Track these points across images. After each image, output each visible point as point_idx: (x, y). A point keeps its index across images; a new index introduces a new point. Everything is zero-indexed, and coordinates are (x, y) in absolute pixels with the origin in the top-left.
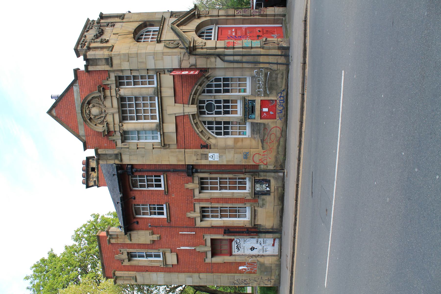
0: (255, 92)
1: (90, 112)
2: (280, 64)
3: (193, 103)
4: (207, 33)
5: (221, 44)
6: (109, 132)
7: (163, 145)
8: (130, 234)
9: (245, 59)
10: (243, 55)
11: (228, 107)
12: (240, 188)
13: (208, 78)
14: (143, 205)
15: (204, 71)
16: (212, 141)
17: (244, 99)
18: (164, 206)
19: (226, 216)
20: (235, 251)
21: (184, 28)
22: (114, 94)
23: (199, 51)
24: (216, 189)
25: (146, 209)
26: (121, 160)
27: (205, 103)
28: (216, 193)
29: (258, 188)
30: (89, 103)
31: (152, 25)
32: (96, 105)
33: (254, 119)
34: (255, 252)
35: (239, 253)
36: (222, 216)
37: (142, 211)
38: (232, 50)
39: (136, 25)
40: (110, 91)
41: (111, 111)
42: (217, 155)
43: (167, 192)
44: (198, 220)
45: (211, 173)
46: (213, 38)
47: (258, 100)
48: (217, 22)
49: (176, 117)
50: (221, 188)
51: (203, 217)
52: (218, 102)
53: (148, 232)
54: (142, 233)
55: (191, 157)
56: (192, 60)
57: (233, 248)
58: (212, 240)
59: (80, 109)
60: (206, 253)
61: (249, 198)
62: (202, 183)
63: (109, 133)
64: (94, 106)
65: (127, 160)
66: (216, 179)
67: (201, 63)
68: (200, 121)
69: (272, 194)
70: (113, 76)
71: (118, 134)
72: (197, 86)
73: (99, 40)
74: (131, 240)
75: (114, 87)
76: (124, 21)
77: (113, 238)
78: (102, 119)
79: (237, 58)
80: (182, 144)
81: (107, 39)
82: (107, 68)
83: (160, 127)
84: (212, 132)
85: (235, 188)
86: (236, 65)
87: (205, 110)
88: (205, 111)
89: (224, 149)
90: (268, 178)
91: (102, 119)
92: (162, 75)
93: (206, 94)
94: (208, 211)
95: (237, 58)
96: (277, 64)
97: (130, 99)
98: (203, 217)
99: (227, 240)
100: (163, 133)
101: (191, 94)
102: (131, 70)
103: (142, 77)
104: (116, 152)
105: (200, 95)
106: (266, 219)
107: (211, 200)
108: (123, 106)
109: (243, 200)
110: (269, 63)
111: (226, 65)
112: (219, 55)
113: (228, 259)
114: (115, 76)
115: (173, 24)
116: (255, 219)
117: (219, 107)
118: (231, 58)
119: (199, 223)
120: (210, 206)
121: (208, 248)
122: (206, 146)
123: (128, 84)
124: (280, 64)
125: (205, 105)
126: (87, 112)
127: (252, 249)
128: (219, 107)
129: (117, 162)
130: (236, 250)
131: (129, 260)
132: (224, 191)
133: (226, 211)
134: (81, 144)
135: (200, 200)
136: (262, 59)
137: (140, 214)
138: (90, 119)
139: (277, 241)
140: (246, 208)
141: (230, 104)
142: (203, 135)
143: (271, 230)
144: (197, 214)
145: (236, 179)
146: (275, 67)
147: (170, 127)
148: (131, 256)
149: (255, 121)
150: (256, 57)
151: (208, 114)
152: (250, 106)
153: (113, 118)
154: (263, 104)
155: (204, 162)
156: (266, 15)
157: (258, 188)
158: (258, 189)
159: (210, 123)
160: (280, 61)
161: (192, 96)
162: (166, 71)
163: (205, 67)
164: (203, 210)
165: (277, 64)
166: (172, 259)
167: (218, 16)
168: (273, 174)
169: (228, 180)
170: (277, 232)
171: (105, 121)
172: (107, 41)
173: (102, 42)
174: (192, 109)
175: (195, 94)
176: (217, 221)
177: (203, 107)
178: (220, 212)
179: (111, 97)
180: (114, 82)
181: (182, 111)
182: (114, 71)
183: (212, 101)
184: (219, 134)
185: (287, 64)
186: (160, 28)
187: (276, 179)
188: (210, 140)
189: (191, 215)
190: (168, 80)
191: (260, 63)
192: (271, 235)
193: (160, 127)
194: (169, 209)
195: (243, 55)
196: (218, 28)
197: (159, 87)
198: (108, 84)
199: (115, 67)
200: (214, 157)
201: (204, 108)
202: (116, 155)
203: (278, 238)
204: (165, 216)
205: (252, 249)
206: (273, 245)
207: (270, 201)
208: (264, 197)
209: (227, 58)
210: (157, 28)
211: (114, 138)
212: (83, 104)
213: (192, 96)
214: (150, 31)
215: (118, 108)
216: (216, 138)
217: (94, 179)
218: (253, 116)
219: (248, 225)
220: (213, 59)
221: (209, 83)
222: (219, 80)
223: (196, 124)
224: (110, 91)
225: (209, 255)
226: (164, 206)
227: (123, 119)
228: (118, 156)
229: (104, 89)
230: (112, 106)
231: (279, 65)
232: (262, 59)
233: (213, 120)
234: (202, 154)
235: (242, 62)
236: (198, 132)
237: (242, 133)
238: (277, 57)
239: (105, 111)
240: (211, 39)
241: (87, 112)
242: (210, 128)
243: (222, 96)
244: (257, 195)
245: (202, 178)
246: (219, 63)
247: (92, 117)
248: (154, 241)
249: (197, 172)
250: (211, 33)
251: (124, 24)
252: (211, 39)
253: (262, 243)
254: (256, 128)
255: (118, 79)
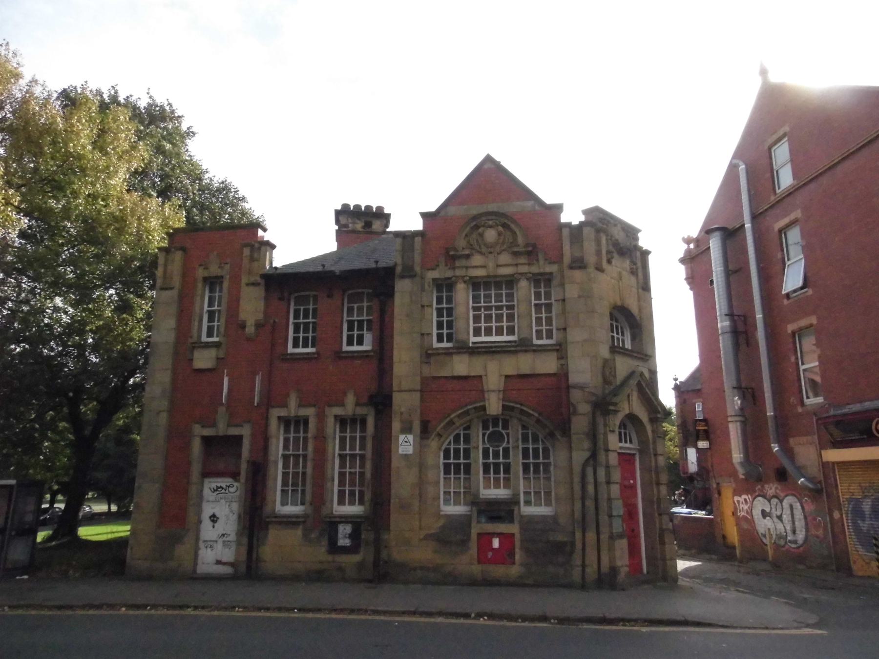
0: (529, 523)
1: (491, 227)
2: (583, 571)
3: (504, 407)
4: (625, 434)
5: (613, 459)
6: (454, 258)
7: (430, 352)
8: (259, 284)
9: (590, 504)
10: (596, 500)
11: (497, 472)
12: (341, 494)
13: (551, 435)
14: (315, 310)
15: (565, 428)
16: (433, 443)
17: (514, 501)
18: (310, 350)
19: (286, 466)
20: (210, 484)
21: (635, 396)
22: (524, 269)
23: (600, 421)
24: (342, 447)
25: (306, 316)
26: (402, 277)
27: (503, 428)
28: (334, 448)
29: (344, 530)
30: (505, 226)
31: (633, 338)
32: (502, 238)
33: (478, 522)
34: (206, 524)
35: (207, 492)
36: (286, 458)
37: (302, 308)
38: (604, 480)
39: (635, 310)
40: (525, 264)
41: (491, 265)
42: (410, 450)
43: (340, 356)
44: (283, 413)
45: (375, 438)
46: (623, 445)
47: (513, 529)
48: (643, 451)
49: (481, 377)
50: (342, 457)
51: (286, 422)
52: (506, 451)
53: (261, 316)
54: (261, 305)
55: (405, 402)
56: (584, 408)
57: (219, 480)
58: (239, 439)
59: (495, 210)
60: (214, 425)
61: (325, 511)
62: (353, 420)
63: (452, 258)
64: (500, 234)
65: (402, 288)
66: (363, 447)
67: (580, 424)
68: (470, 421)
69: (330, 558)
70: (553, 268)
71: (449, 274)
72: (536, 415)
73: (611, 248)
74: (248, 285)
75: (535, 269)
76: (640, 290)
77: (252, 251)
78: (478, 248)
79: (591, 488)
80: (429, 387)
81: (614, 261)
82: (567, 260)
83: (464, 349)
84: (450, 442)
85: (342, 483)
86: (577, 488)
87: (491, 429)
88: (488, 429)
89: (419, 462)
90: (362, 549)
91: (478, 248)
92: (555, 354)
93: (520, 432)
94: (297, 431)
95: (591, 488)
96: (584, 566)
97: (510, 297)
98: (286, 422)
99: (238, 467)
100: (451, 354)
101: (522, 405)
102: (564, 300)
103: (549, 321)
104: (417, 269)
105: (520, 420)
106: (282, 547)
107: (321, 437)
108: (498, 285)
109: (319, 500)
110: (584, 549)
111: (577, 469)
112: (594, 456)
113: (196, 469)
114: (551, 274)
115: (642, 374)
116: (280, 523)
117: (496, 455)
118: (590, 478)
119: (276, 413)
120: (310, 435)
121: (222, 428)
122: (425, 431)
123: (538, 296)
124: (583, 571)
125: (500, 429)
126: (490, 223)
127: (214, 519)
128: (496, 455)
129: (399, 269)
130: (214, 485)
131: (205, 279)
132: (337, 461)
133: (296, 465)
134: (433, 208)
135: (321, 417)
136: (591, 536)
137: (295, 305)
138: (477, 227)
139: (228, 570)
140: (303, 504)
141: (502, 475)
142: (448, 424)
143: (254, 556)
144: (293, 408)
145: (362, 484)
146: (577, 560)
147: (461, 366)
148: (213, 282)
149: (474, 524)
150: (594, 526)
151: (484, 435)
152: (503, 514)
153: (479, 266)
154: (506, 538)
155: (396, 425)
156: (662, 543)
157: (344, 530)
158: (341, 528)
159: (467, 439)
160: (588, 570)
161: (519, 406)
162: (563, 362)
163: (573, 431)
164: (301, 422)
165: (584, 566)
166: (203, 360)
167: (655, 455)
168: (370, 558)
169: (358, 470)
170: (249, 569)
171: (473, 251)
172: (609, 262)
173: (609, 252)
174: (494, 406)
175: (522, 412)
176: (277, 448)
177: (495, 425)
178: (293, 455)
179: (517, 265)
180: (542, 271)
181: (492, 387)
182: (561, 271)
183: (508, 442)
184: (447, 455)
185: (583, 586)
186: (627, 350)
187: (361, 566)
188: (437, 439)
189: (293, 402)
190: (548, 365)
191: (584, 532)
192: (244, 557)
193: (464, 349)
194: (307, 358)
195: (596, 500)
196: (634, 455)
197: (534, 348)
198: (538, 260)
199: (568, 273)
200: (405, 444)
201: (494, 428)
202: (411, 268)
203: (236, 571)
204: (291, 350)
205: (214, 519)
206: (219, 562)
207: (316, 555)
208: (325, 542)
209: (590, 471)
210: (628, 345)
211: (442, 266)
212: (504, 215)
213: (519, 406)
214: (623, 334)
215: (495, 276)
216: (440, 449)
217: (350, 225)
218: (483, 520)
219: (267, 509)
220: (587, 444)
221: (541, 437)
222: (546, 455)
223: (467, 413)
224: (525, 264)
225: (208, 432)
226: (310, 350)
227: (476, 284)
228: (409, 273)
229: (529, 253)
230: (504, 265)
231: (580, 569)
232: (591, 536)
233: (473, 444)
234: (411, 423)
235: (583, 498)
236: (452, 416)
237: (448, 497)
238: (595, 566)
239: (491, 253)
240: (620, 441)
241: (490, 223)
242: (457, 439)
243: (517, 461)
244: (332, 524)
245: (363, 422)
246: (580, 456)
247: (480, 230)
248: (243, 326)
249: (378, 413)
250: (626, 442)
251: (634, 290)
252: (620, 441)
253: (224, 539)
254: (460, 525)
255: (547, 277)
